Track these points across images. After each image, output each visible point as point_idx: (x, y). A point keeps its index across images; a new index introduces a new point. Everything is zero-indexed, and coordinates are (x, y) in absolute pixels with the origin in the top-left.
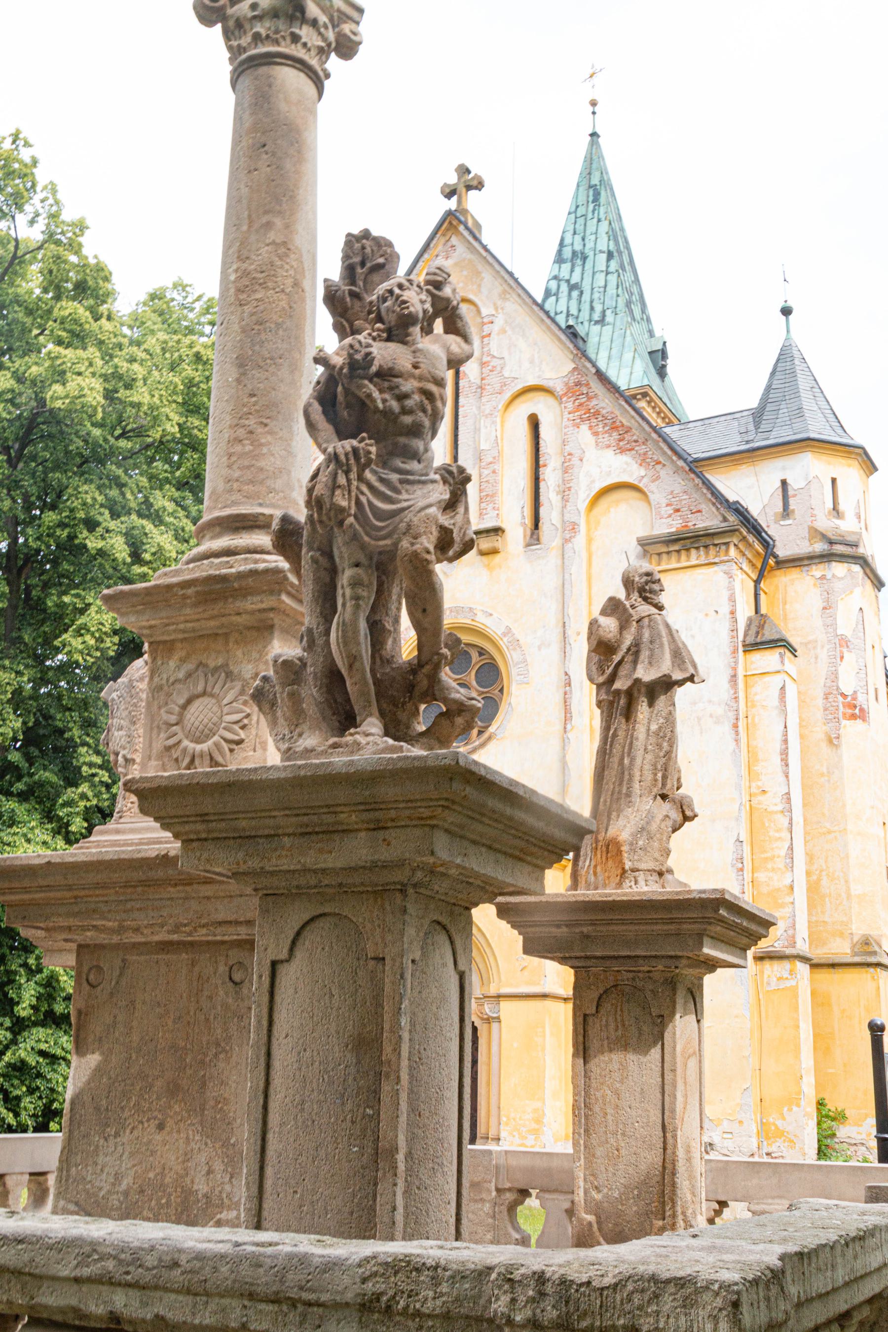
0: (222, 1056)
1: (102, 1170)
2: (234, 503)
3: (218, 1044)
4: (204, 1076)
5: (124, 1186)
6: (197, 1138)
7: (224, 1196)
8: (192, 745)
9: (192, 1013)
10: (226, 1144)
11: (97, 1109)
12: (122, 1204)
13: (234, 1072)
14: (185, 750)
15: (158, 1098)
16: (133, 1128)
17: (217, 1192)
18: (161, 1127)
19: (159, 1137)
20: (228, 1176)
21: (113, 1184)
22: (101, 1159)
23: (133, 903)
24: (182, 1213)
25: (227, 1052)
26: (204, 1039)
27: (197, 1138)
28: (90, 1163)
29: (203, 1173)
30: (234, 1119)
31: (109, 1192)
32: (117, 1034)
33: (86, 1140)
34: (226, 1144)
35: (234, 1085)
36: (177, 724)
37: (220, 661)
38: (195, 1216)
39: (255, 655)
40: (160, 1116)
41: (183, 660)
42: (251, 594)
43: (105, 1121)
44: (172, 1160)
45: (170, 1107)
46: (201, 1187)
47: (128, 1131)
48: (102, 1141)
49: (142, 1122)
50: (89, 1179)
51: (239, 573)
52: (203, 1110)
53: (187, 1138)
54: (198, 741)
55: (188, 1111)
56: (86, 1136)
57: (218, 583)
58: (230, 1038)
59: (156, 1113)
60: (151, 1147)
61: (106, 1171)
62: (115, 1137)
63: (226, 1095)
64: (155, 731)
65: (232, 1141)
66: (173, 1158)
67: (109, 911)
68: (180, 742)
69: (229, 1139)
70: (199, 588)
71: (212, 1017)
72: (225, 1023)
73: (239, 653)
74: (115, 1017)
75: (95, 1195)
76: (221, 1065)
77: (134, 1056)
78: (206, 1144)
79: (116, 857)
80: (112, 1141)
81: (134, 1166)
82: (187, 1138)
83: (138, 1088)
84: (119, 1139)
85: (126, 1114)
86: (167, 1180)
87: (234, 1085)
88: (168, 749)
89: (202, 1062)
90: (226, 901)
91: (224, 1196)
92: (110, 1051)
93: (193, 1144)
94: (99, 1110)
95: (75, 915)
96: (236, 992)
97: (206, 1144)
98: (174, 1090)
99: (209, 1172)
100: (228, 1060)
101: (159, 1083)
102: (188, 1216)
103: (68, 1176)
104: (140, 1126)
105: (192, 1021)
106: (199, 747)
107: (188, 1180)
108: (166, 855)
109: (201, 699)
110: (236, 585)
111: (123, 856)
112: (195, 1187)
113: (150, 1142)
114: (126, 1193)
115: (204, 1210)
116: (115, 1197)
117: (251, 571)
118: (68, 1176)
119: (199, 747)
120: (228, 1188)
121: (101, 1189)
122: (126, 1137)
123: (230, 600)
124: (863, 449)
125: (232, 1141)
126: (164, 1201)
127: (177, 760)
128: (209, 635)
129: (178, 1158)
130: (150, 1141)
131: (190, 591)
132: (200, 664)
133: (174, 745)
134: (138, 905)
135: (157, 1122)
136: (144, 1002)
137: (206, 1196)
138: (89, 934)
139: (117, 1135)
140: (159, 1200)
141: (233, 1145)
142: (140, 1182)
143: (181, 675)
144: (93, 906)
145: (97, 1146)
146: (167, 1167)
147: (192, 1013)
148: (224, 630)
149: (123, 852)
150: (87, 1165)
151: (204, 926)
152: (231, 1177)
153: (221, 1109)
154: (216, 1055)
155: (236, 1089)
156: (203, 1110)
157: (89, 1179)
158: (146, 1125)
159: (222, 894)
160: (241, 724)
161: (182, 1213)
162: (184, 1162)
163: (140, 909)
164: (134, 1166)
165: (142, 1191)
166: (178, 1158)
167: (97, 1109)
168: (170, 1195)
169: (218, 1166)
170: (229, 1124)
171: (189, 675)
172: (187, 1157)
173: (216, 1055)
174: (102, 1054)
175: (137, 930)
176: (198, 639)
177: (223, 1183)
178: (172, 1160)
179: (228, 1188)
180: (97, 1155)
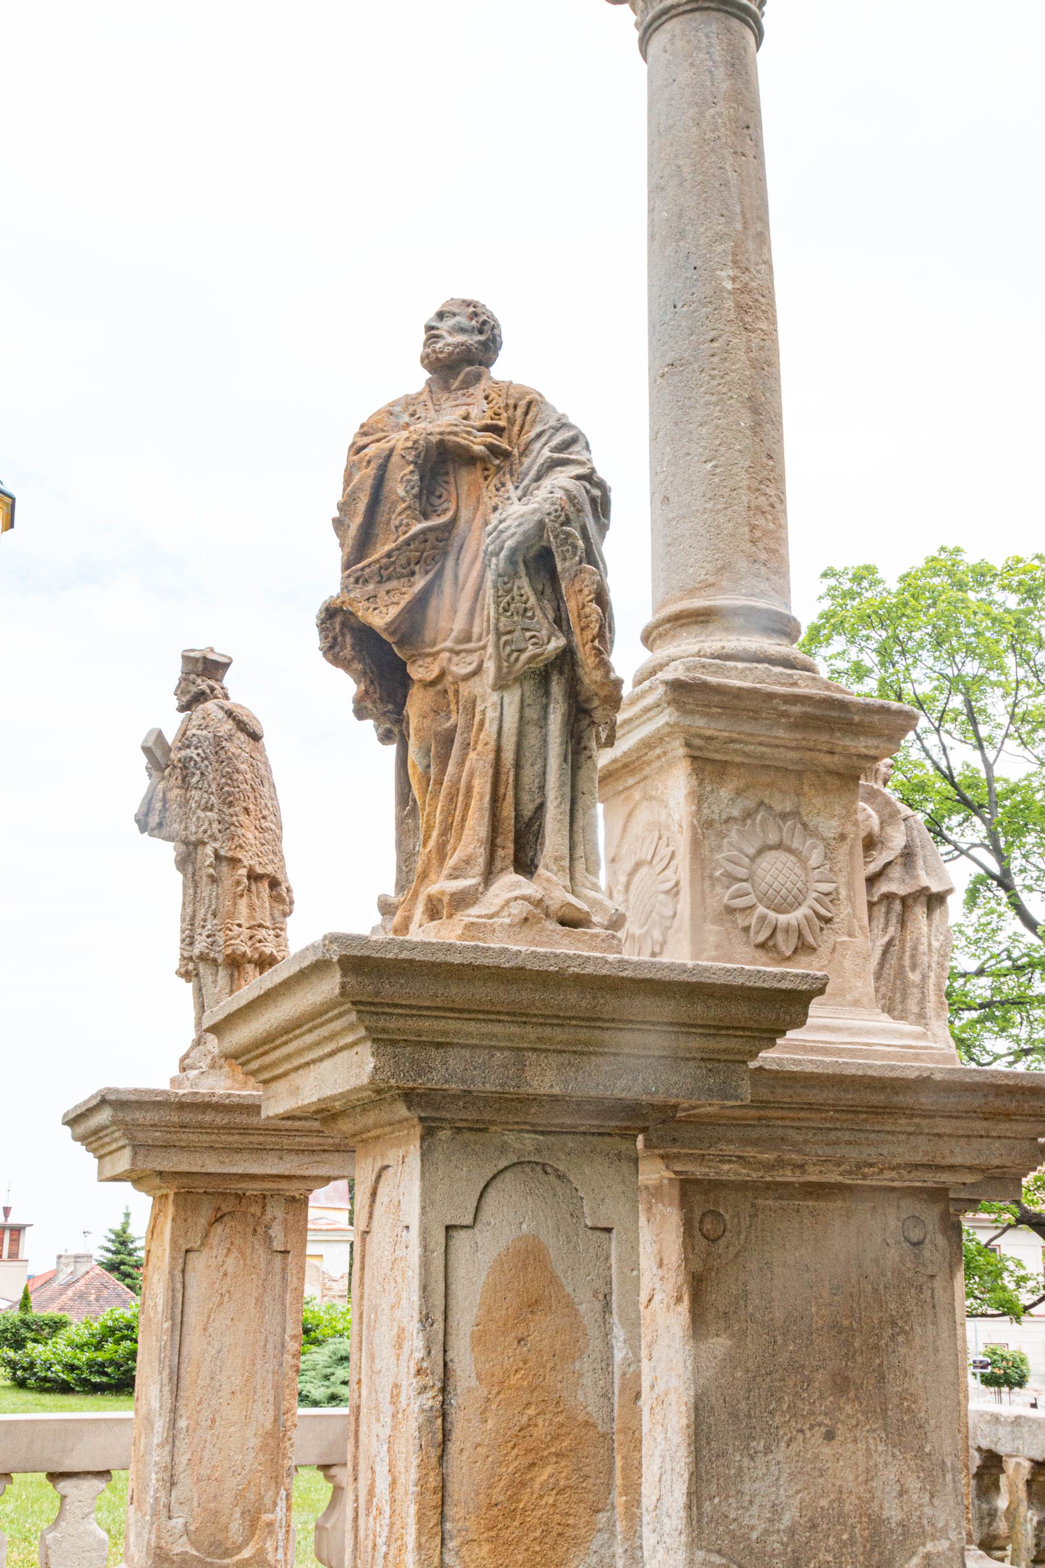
0: (900, 1339)
1: (751, 1502)
2: (763, 594)
3: (894, 1324)
4: (881, 1365)
5: (786, 1520)
6: (880, 1449)
7: (925, 1522)
8: (772, 915)
9: (853, 1281)
10: (920, 1454)
11: (734, 1416)
12: (785, 1545)
13: (919, 1360)
14: (763, 919)
15: (821, 1397)
16: (790, 1440)
17: (915, 1518)
18: (830, 1436)
19: (827, 1450)
20: (927, 1496)
21: (771, 1521)
22: (747, 1487)
23: (839, 1134)
24: (872, 1550)
25: (906, 1333)
26: (875, 1317)
27: (880, 1449)
28: (732, 1493)
29: (894, 1494)
30: (927, 1421)
31: (766, 1531)
32: (750, 1309)
33: (721, 1461)
34: (920, 1454)
35: (920, 1376)
36: (745, 881)
37: (788, 806)
38: (891, 1552)
39: (838, 810)
40: (827, 1421)
41: (739, 792)
42: (865, 733)
43: (747, 1432)
44: (848, 1478)
45: (841, 1409)
46: (893, 1512)
47: (783, 1444)
48: (746, 1462)
49: (802, 1431)
50: (732, 1516)
51: (867, 705)
52: (886, 1410)
53: (868, 1450)
54: (778, 910)
55: (865, 1413)
56: (721, 1455)
57: (834, 709)
58: (909, 1314)
59: (821, 1418)
60: (819, 1465)
61: (758, 1500)
62: (766, 1454)
63: (911, 1391)
64: (707, 883)
65: (927, 1450)
66: (851, 1478)
67: (806, 1142)
68: (752, 907)
69: (921, 1448)
70: (809, 710)
71: (881, 1287)
72: (900, 1295)
73: (818, 801)
74: (745, 1284)
75: (745, 1538)
76: (903, 1350)
77: (780, 1339)
78: (894, 1456)
79: (860, 1073)
80: (760, 1459)
81: (797, 1492)
82: (868, 1450)
83: (791, 1383)
84: (770, 1457)
85: (778, 1419)
86: (847, 1507)
87: (920, 1376)
88: (730, 911)
89: (876, 1347)
90: (963, 1141)
91: (925, 1522)
92: (744, 1332)
93: (875, 1456)
94: (737, 1416)
95: (755, 1143)
96: (916, 1256)
97: (894, 1456)
98: (841, 1385)
99: (902, 1493)
100: (909, 1342)
101: (820, 1376)
102: (881, 1554)
103: (700, 1515)
104: (800, 1437)
105: (855, 1291)
106: (783, 918)
107: (875, 1505)
108: (928, 1077)
109: (773, 853)
110: (857, 718)
111: (870, 1072)
112: (886, 1514)
113: (816, 1457)
114: (792, 1532)
115: (902, 1543)
116: (775, 1537)
117: (882, 707)
118: (700, 1515)
119: (783, 918)
120: (928, 1510)
121: (752, 1528)
122: (780, 1454)
123: (838, 734)
124: (13, 499)
125: (927, 1450)
126: (845, 1537)
127: (746, 929)
128: (777, 769)
129: (857, 1477)
130: (816, 1457)
131: (797, 709)
132: (762, 803)
133: (743, 910)
134: (847, 1136)
135: (823, 1429)
136: (785, 1265)
137: (901, 1524)
138: (726, 1167)
139: (767, 1450)
140: (838, 1537)
141: (929, 1454)
142: (809, 1514)
143: (736, 813)
144: (780, 1132)
145: (740, 1469)
146: (844, 1491)
147: (853, 1281)
148: (799, 768)
149: (870, 1067)
150: (728, 1496)
151: (894, 1169)
152: (932, 1497)
153: (909, 1408)
154: (893, 1338)
155: (924, 1381)
156: (885, 1410)
157: (732, 1516)
158: (808, 1434)
159: (961, 1132)
160: (831, 897)
161: (872, 1550)
162: (866, 1482)
163: (849, 1143)
164: (797, 1492)
165: (814, 1526)
166: (857, 1477)
167: (734, 1416)
168: (853, 1527)
169: (913, 1484)
170: (921, 1427)
171: (748, 815)
172: (870, 1474)
173: (893, 1338)
174: (732, 1336)
175: (801, 1167)
176: (764, 770)
177: (921, 1505)
178: (848, 1478)
179: (928, 1510)
180: (742, 1481)
